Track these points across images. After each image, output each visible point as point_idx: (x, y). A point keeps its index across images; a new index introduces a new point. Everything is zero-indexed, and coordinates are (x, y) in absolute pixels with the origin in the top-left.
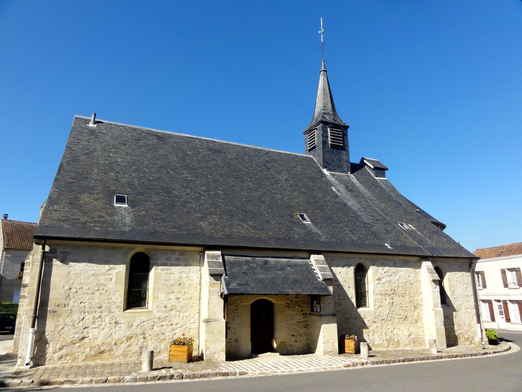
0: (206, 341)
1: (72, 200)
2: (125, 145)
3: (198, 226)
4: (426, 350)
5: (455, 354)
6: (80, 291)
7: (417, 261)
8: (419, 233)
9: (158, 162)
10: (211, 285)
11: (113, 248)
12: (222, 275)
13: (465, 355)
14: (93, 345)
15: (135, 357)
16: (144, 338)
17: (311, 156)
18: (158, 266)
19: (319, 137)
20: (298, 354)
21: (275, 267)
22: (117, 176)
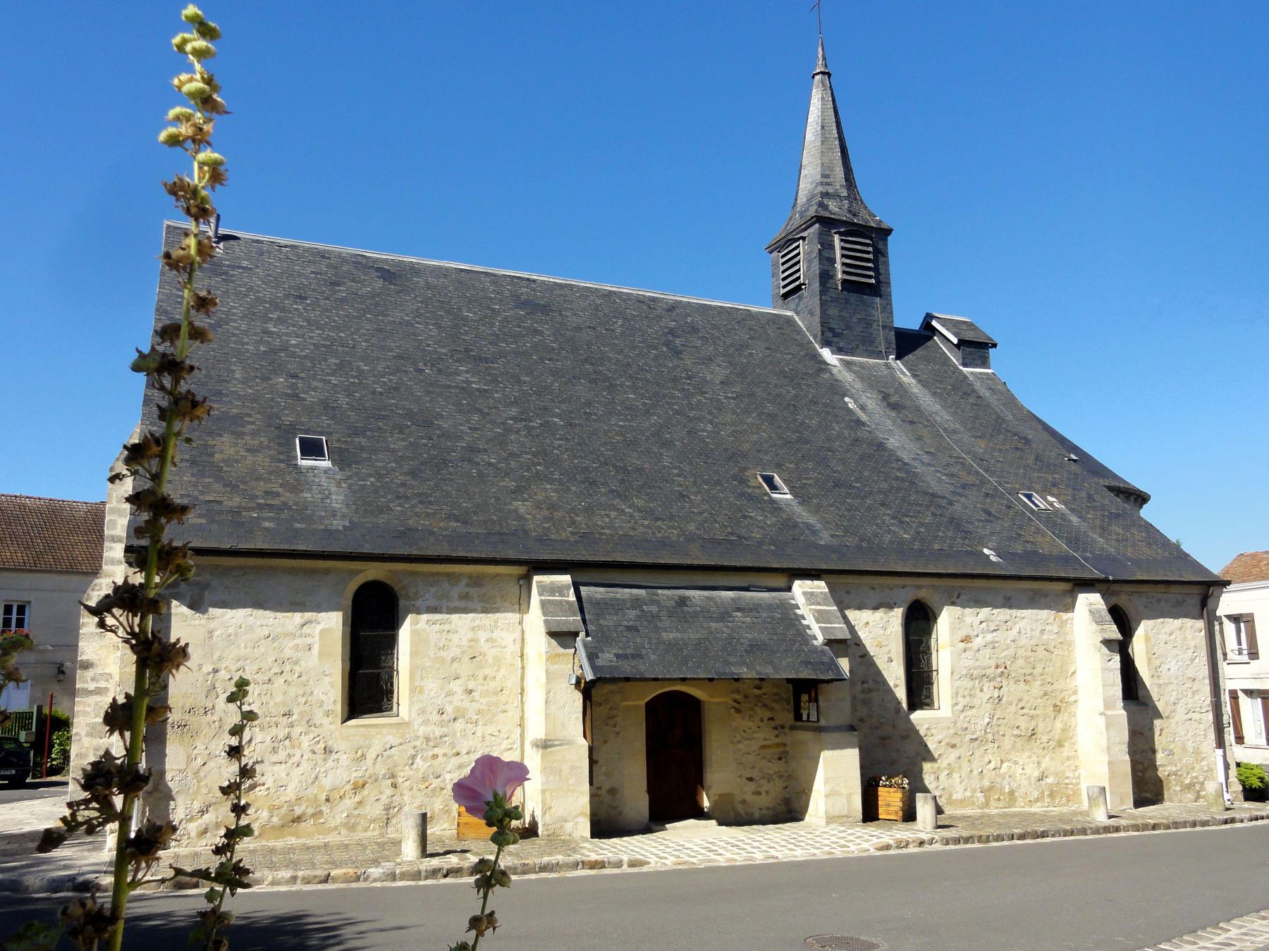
0: (543, 792)
1: (194, 453)
2: (302, 298)
3: (510, 512)
4: (1081, 813)
5: (1152, 822)
7: (1066, 592)
8: (1074, 519)
9: (389, 343)
10: (551, 658)
11: (310, 572)
12: (576, 634)
13: (1176, 825)
14: (276, 803)
15: (374, 829)
16: (394, 786)
17: (789, 313)
18: (419, 613)
19: (810, 261)
20: (763, 822)
21: (705, 613)
22: (293, 386)
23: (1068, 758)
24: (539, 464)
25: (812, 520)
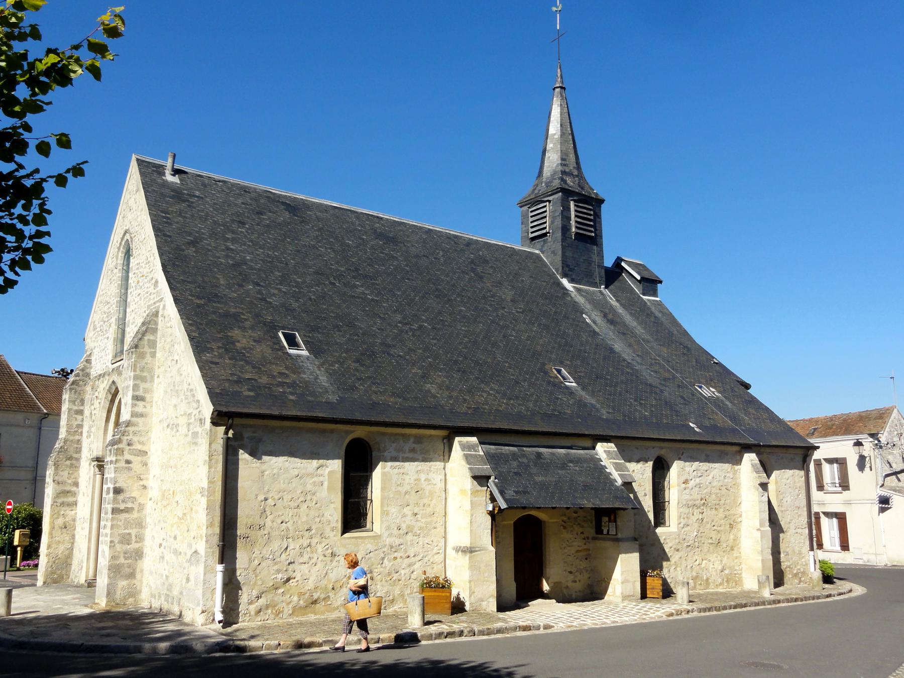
0: (470, 581)
6: (279, 504)
8: (728, 403)
11: (323, 431)
17: (537, 252)
19: (553, 219)
23: (736, 558)
24: (428, 357)
25: (593, 402)
